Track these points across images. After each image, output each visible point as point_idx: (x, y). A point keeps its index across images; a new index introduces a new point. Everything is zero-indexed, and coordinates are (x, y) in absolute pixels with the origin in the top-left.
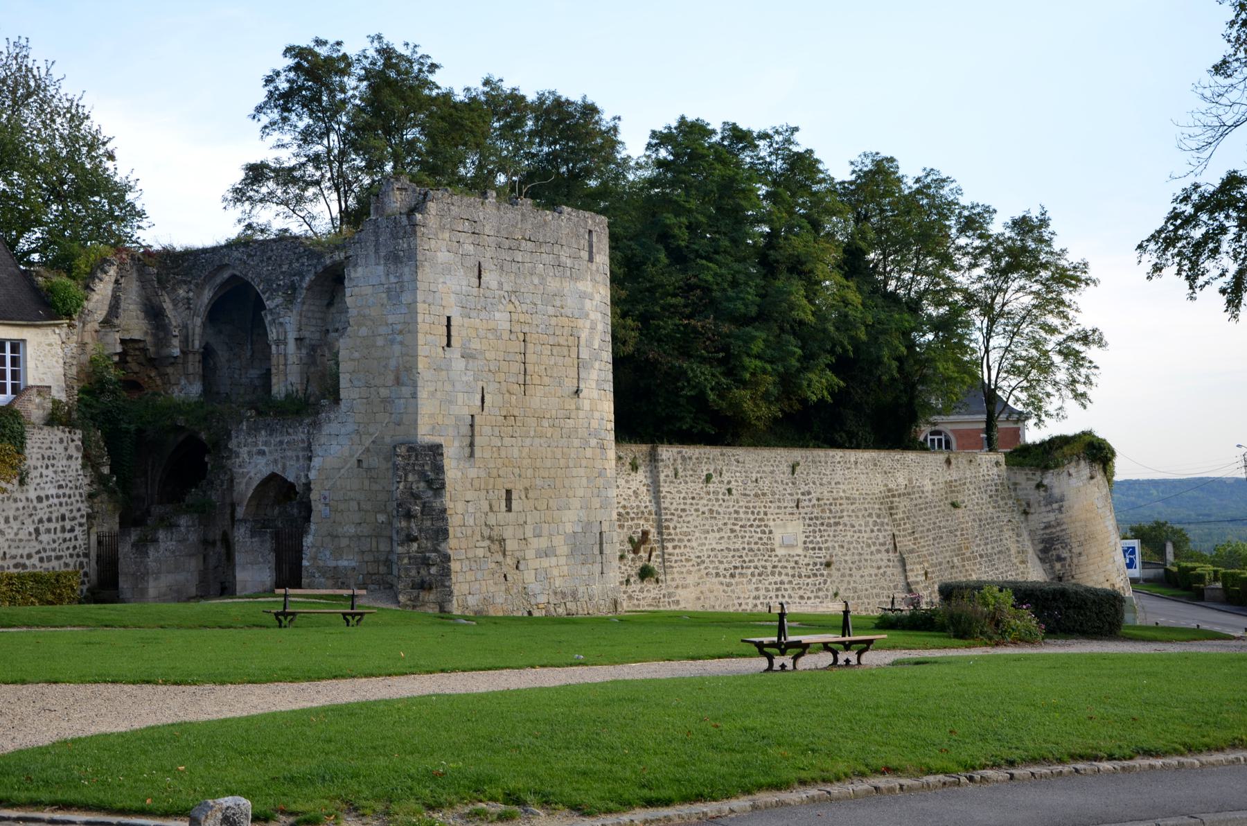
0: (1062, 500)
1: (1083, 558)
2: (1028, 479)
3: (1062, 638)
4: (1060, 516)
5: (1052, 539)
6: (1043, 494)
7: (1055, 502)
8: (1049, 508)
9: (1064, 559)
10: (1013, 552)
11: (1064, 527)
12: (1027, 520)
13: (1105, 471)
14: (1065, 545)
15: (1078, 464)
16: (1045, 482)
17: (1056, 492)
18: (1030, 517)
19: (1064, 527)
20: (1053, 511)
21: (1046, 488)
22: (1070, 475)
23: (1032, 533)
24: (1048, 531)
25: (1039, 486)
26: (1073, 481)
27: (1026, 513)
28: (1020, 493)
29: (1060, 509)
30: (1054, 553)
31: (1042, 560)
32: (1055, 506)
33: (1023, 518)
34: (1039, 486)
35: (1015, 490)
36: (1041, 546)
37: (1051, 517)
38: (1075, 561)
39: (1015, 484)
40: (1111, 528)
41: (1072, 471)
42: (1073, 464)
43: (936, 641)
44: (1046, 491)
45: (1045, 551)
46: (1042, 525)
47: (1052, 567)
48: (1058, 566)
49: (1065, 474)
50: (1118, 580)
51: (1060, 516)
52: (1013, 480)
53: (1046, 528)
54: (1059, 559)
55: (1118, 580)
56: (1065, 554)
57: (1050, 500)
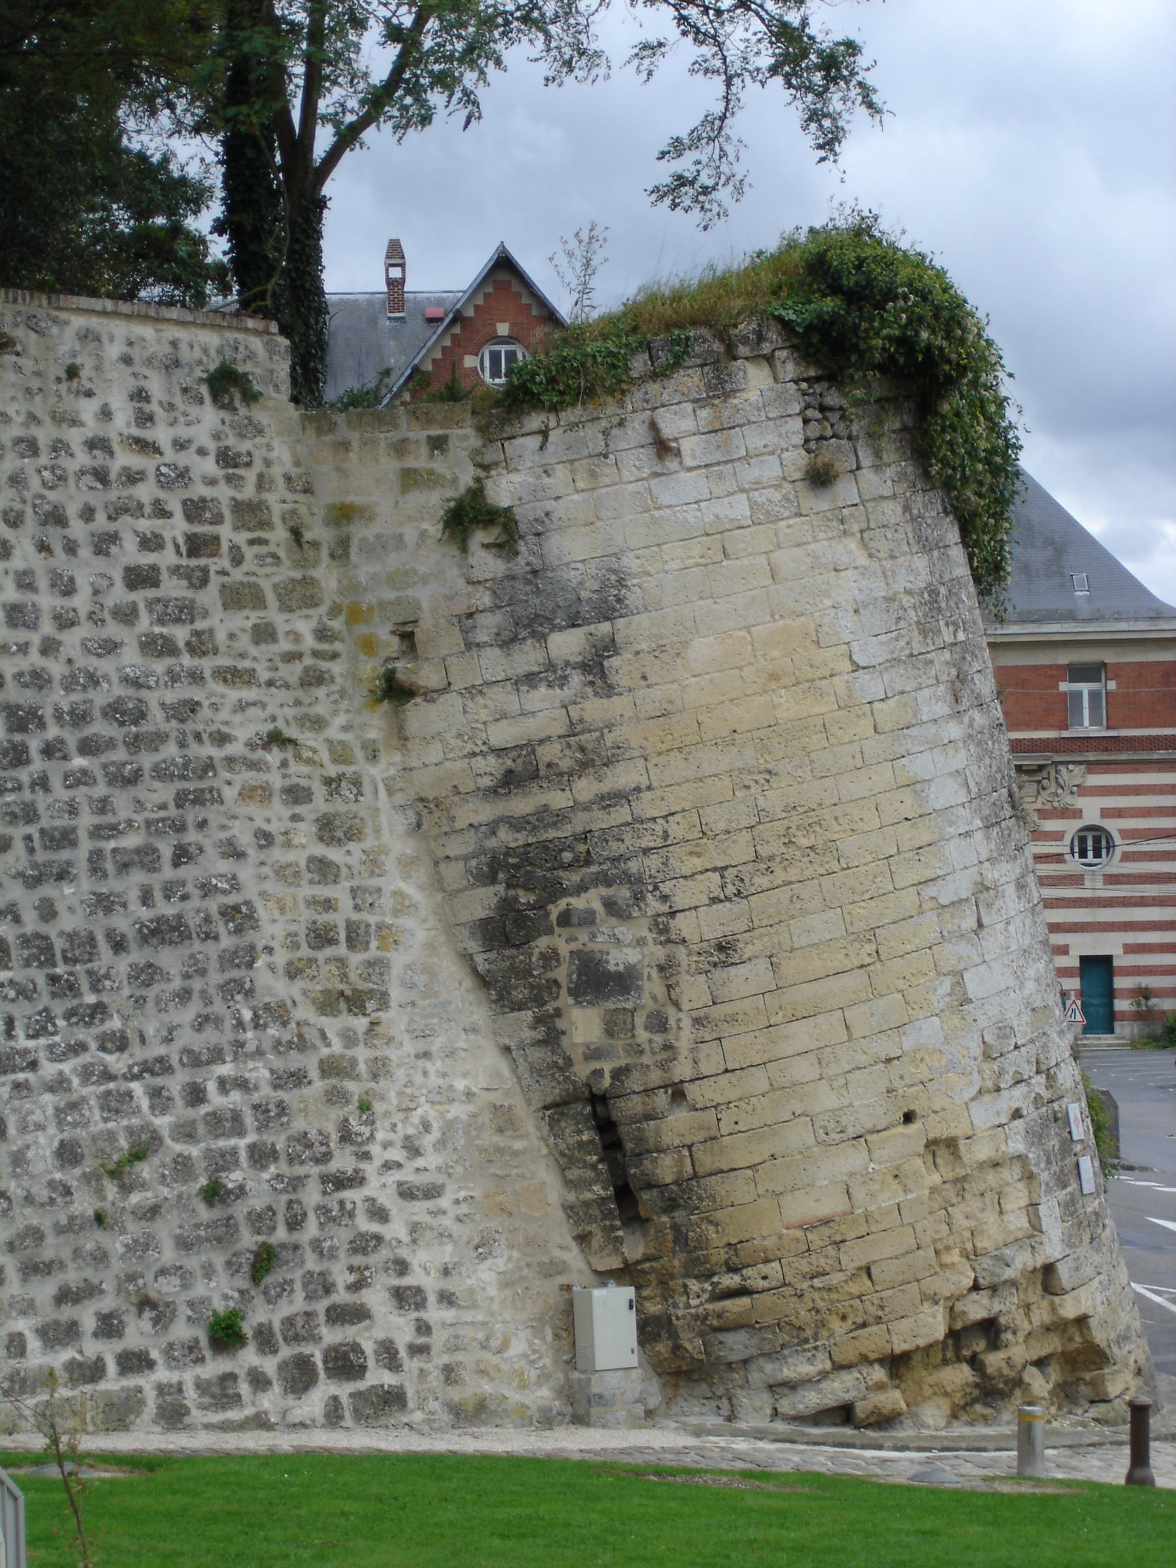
0: (608, 611)
1: (746, 978)
2: (410, 479)
3: (149, 1452)
4: (595, 709)
5: (550, 852)
6: (487, 564)
7: (563, 620)
8: (528, 657)
9: (625, 982)
10: (272, 928)
11: (622, 777)
12: (401, 736)
13: (921, 451)
14: (631, 890)
15: (720, 388)
16: (503, 491)
17: (573, 553)
18: (418, 715)
19: (622, 777)
20: (551, 673)
21: (506, 529)
22: (663, 447)
23: (426, 812)
24: (522, 805)
25: (468, 516)
26: (684, 488)
27: (395, 691)
28: (364, 570)
29: (595, 666)
30: (562, 943)
31: (496, 988)
32: (567, 644)
33: (375, 725)
34: (468, 516)
35: (341, 552)
36: (482, 902)
37: (542, 713)
38: (694, 991)
39: (343, 515)
40: (946, 793)
41: (677, 422)
42: (690, 380)
43: (626, 1459)
44: (506, 547)
45: (506, 930)
46: (492, 766)
47: (551, 1035)
48: (584, 1025)
49: (636, 431)
50: (984, 1115)
51: (595, 709)
52: (330, 492)
53: (510, 782)
54: (596, 981)
55: (984, 1115)
56: (626, 947)
57: (532, 610)
